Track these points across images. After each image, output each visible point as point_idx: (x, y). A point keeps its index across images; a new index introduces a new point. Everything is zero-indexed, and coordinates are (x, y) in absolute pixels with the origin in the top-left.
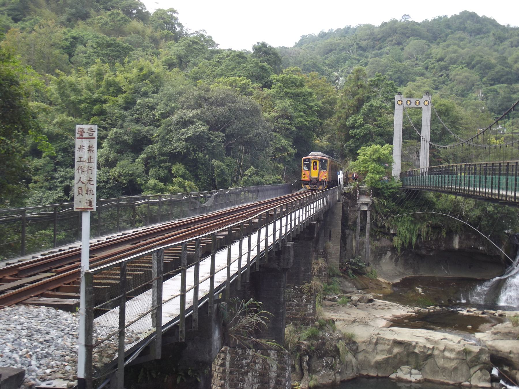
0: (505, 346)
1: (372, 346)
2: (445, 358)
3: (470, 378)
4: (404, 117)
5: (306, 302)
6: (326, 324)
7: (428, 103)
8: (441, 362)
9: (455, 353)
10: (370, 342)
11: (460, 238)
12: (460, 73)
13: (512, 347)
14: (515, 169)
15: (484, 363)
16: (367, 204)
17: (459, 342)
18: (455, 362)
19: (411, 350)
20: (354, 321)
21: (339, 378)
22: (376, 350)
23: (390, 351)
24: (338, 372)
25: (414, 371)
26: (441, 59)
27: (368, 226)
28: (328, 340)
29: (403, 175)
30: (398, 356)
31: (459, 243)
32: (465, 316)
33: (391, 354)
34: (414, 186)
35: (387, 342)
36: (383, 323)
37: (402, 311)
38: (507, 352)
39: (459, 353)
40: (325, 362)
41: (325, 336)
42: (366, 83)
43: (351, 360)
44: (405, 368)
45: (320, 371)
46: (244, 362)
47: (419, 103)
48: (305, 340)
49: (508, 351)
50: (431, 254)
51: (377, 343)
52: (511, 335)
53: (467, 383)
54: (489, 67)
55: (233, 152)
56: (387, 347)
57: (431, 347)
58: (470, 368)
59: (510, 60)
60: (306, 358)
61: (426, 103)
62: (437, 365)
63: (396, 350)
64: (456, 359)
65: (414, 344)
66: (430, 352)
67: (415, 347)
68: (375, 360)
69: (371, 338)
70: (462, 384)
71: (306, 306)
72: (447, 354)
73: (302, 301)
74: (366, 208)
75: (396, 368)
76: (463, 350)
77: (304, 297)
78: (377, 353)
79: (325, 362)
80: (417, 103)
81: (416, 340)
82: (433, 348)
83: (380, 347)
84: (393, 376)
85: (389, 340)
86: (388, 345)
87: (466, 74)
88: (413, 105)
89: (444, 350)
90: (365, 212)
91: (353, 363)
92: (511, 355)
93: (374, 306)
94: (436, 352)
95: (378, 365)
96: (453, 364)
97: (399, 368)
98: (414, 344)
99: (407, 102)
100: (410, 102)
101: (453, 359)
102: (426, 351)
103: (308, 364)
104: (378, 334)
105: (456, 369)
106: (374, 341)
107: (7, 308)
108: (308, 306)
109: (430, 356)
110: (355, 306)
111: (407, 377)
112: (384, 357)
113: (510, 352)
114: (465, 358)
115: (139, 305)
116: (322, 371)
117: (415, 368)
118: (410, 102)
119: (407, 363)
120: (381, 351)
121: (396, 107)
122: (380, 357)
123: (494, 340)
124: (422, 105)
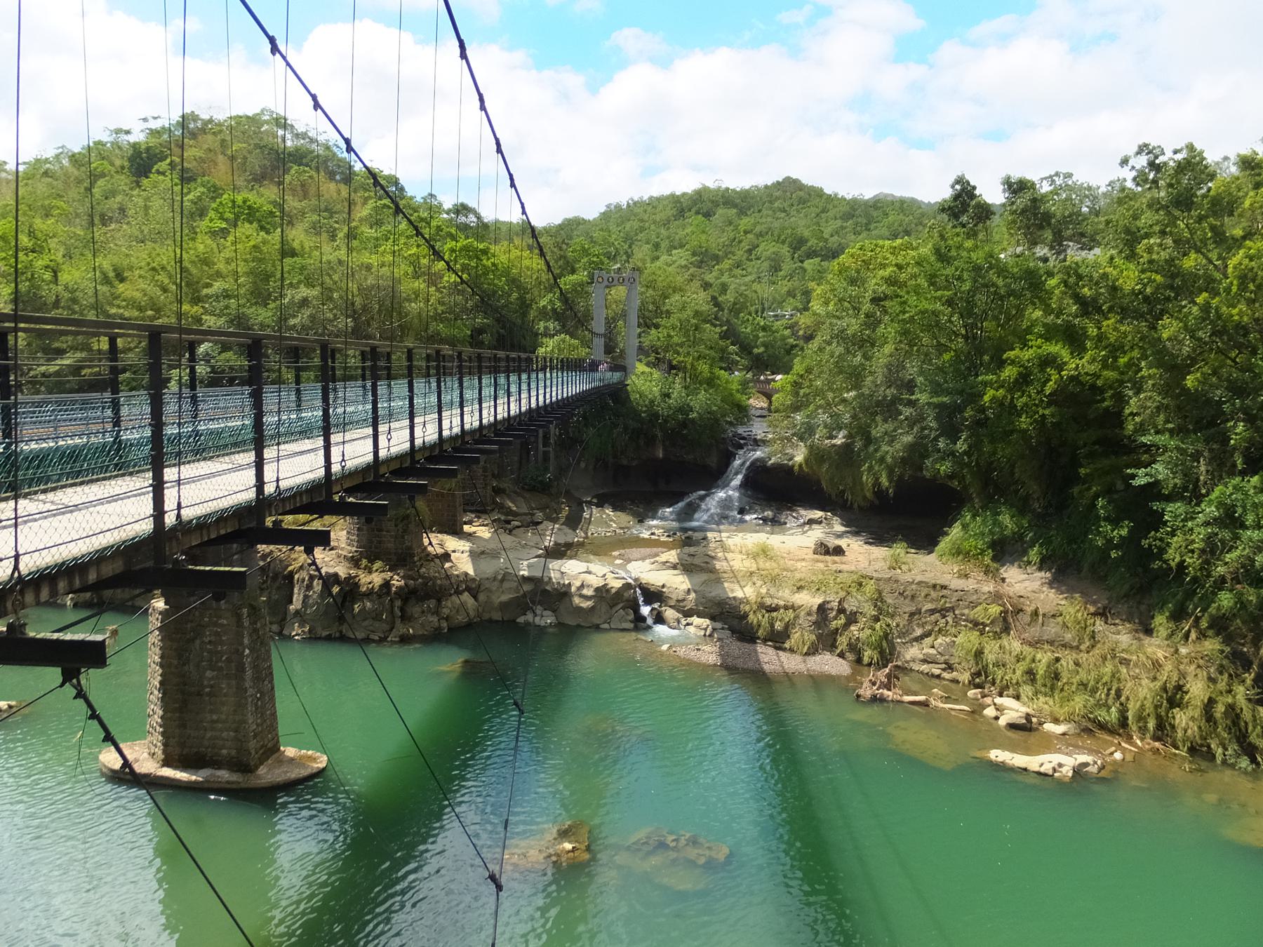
2: (582, 596)
10: (495, 579)
12: (767, 248)
20: (483, 553)
23: (517, 590)
34: (129, 336)
46: (189, 626)
51: (502, 580)
54: (801, 241)
55: (855, 377)
58: (611, 607)
59: (827, 233)
60: (398, 603)
67: (547, 583)
69: (497, 573)
72: (585, 592)
83: (506, 585)
84: (521, 620)
87: (775, 249)
95: (504, 606)
96: (589, 604)
103: (402, 609)
107: (609, 511)
113: (663, 586)
122: (505, 598)
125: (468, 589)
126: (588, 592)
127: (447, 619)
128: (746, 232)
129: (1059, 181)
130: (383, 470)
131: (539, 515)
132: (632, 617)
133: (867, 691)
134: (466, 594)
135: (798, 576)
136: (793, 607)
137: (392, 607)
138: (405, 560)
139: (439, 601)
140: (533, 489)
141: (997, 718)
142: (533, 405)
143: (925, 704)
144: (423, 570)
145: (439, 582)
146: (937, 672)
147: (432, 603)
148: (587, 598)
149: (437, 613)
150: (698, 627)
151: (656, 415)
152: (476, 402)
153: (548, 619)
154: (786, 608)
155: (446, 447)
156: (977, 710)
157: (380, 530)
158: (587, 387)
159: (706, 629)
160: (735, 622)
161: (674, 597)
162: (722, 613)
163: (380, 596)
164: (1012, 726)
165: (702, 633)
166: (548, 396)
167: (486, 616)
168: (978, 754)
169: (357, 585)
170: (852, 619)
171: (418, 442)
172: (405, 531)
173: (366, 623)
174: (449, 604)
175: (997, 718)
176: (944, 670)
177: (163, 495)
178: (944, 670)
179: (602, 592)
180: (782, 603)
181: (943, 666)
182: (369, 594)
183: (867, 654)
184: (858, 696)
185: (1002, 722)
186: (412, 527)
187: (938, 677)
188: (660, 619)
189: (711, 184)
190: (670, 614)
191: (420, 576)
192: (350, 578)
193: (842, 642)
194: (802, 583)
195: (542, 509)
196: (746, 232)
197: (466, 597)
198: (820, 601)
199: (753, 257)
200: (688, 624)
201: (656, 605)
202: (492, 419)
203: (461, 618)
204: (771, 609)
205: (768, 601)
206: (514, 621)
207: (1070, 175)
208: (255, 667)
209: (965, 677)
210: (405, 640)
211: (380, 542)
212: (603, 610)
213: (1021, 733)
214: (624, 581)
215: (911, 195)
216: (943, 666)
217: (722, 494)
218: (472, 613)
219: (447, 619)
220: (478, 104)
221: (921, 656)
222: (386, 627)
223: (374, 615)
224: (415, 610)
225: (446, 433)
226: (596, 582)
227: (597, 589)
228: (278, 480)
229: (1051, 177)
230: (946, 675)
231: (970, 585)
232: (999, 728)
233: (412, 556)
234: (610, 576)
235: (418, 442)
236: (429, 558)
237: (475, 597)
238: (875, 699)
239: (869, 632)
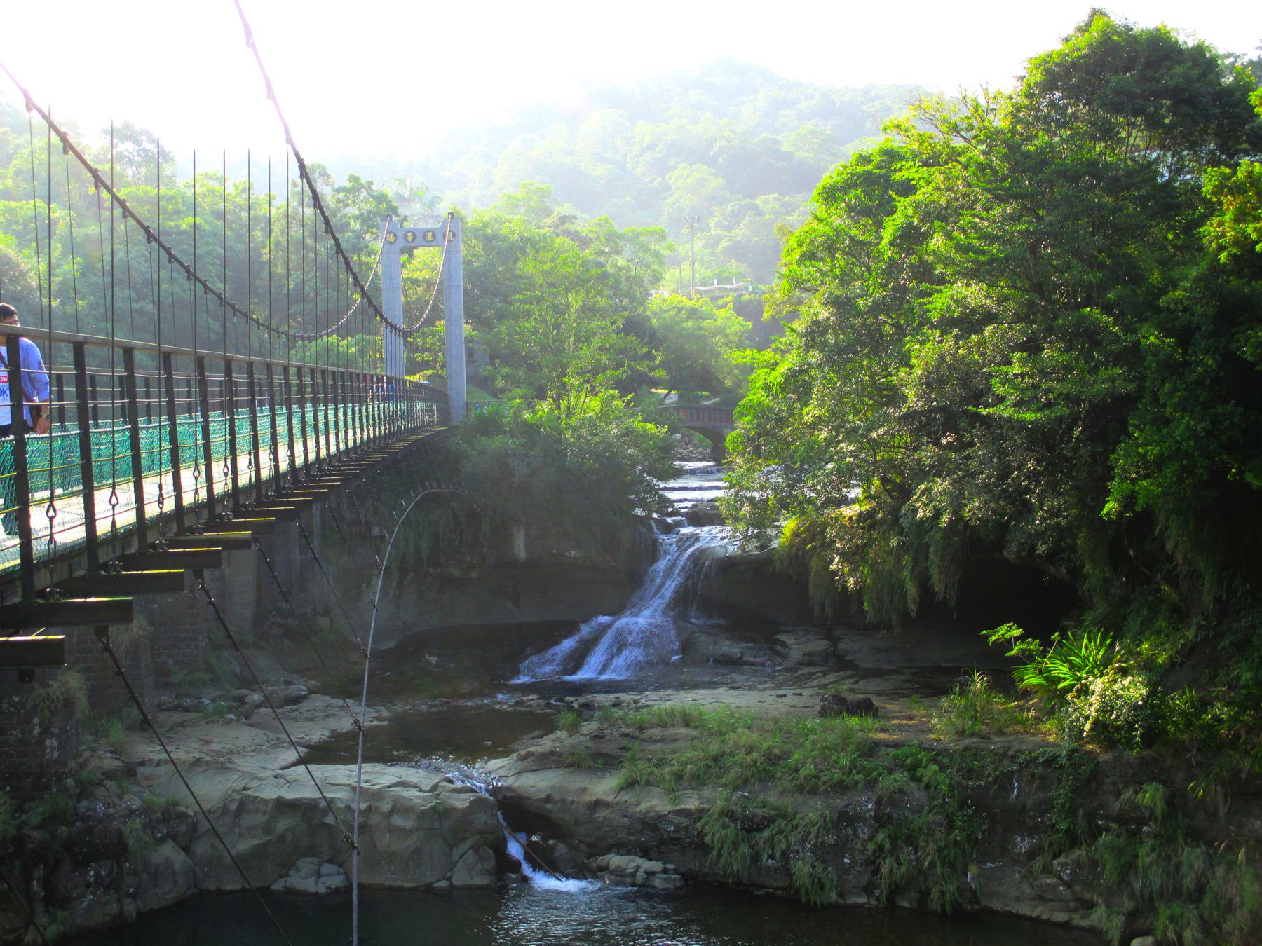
1: (228, 819)
2: (393, 830)
3: (451, 870)
5: (41, 733)
6: (102, 780)
9: (414, 817)
10: (224, 811)
11: (527, 535)
13: (553, 788)
14: (70, 389)
15: (480, 832)
21: (130, 908)
22: (239, 826)
23: (267, 829)
24: (128, 895)
25: (327, 868)
26: (652, 147)
28: (100, 821)
30: (289, 837)
31: (526, 546)
33: (269, 834)
35: (261, 807)
38: (541, 800)
39: (423, 815)
40: (92, 873)
41: (95, 810)
44: (306, 864)
45: (83, 895)
48: (36, 828)
49: (543, 796)
50: (474, 575)
52: (554, 758)
53: (444, 884)
56: (260, 819)
57: (363, 806)
58: (451, 847)
60: (39, 872)
62: (376, 848)
63: (283, 825)
64: (418, 830)
67: (325, 812)
69: (227, 800)
71: (41, 742)
72: (398, 821)
73: (31, 731)
75: (287, 865)
76: (433, 808)
77: (36, 720)
78: (241, 835)
79: (92, 873)
82: (369, 809)
84: (278, 886)
85: (266, 802)
86: (264, 813)
89: (392, 812)
91: (177, 866)
92: (549, 806)
94: (375, 819)
96: (411, 843)
97: (294, 864)
99: (406, 236)
101: (411, 831)
104: (245, 789)
105: (417, 851)
106: (233, 807)
108: (48, 743)
110: (246, 718)
111: (309, 885)
112: (256, 842)
113: (548, 799)
114: (437, 825)
116: (85, 896)
117: (330, 861)
119: (310, 852)
120: (249, 829)
123: (519, 772)
130: (103, 556)
132: (490, 864)
142: (299, 461)
148: (406, 833)
151: (251, 265)
152: (167, 467)
155: (43, 580)
158: (353, 438)
166: (358, 435)
171: (103, 528)
177: (85, 508)
202: (203, 495)
206: (268, 888)
214: (471, 796)
220: (265, 91)
225: (151, 511)
228: (51, 535)
231: (313, 347)
235: (103, 528)
237: (186, 850)
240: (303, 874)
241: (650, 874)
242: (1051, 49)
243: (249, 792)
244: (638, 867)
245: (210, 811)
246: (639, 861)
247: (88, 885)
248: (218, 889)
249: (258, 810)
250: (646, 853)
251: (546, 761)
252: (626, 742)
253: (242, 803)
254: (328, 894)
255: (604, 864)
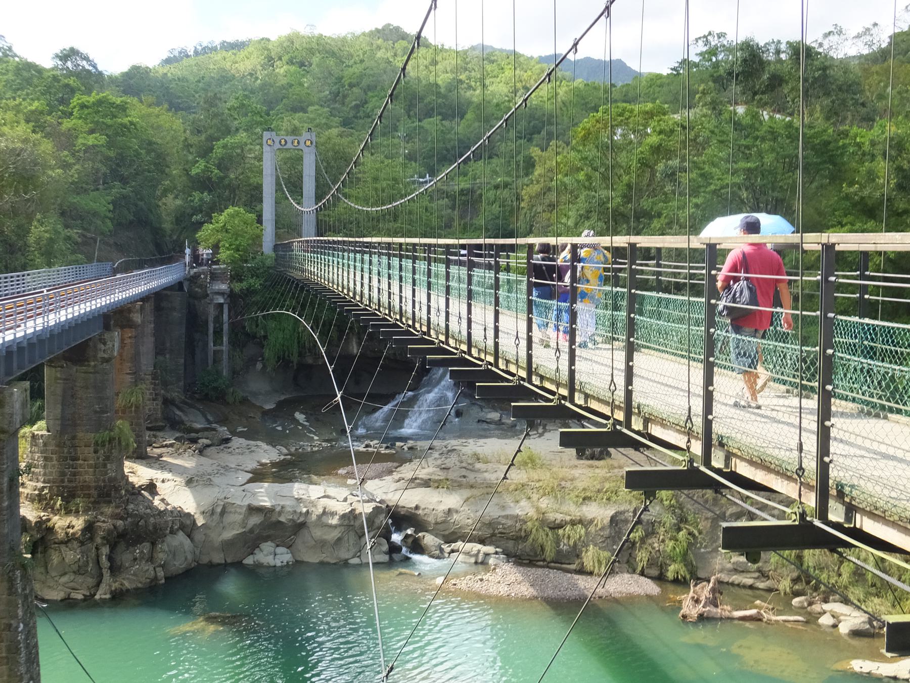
0: (410, 499)
4: (126, 268)
7: (311, 143)
8: (318, 533)
9: (338, 517)
16: (221, 293)
17: (345, 500)
18: (339, 529)
19: (273, 519)
23: (244, 523)
25: (281, 550)
27: (226, 327)
29: (276, 248)
32: (362, 452)
36: (245, 477)
37: (268, 454)
42: (224, 107)
43: (181, 544)
44: (268, 546)
47: (298, 143)
51: (223, 512)
60: (105, 550)
61: (308, 143)
64: (340, 525)
65: (278, 509)
66: (302, 519)
67: (280, 513)
68: (220, 539)
70: (837, 248)
74: (221, 301)
80: (296, 144)
81: (282, 503)
84: (249, 561)
88: (289, 145)
90: (221, 305)
91: (186, 547)
93: (230, 450)
95: (228, 545)
98: (278, 509)
99: (280, 142)
100: (286, 142)
102: (296, 518)
103: (110, 558)
105: (339, 539)
106: (219, 510)
109: (302, 526)
113: (417, 507)
114: (352, 523)
115: (63, 312)
118: (286, 142)
121: (266, 148)
122: (228, 535)
124: (302, 146)
125: (182, 527)
126: (334, 521)
127: (163, 566)
128: (351, 86)
129: (714, 42)
131: (223, 431)
133: (690, 609)
134: (181, 533)
135: (580, 485)
136: (581, 522)
137: (98, 556)
138: (109, 495)
139: (153, 544)
140: (206, 398)
141: (835, 626)
143: (757, 619)
144: (131, 506)
145: (152, 520)
146: (749, 581)
147: (146, 547)
149: (151, 559)
150: (468, 554)
153: (283, 557)
154: (573, 523)
156: (812, 619)
157: (75, 459)
159: (477, 555)
160: (511, 544)
161: (431, 519)
162: (493, 535)
163: (82, 543)
164: (856, 633)
165: (473, 560)
167: (205, 560)
168: (839, 666)
169: (51, 530)
170: (651, 532)
172: (107, 458)
173: (64, 579)
174: (165, 547)
175: (835, 626)
176: (757, 578)
178: (757, 578)
179: (351, 517)
180: (568, 518)
181: (757, 575)
182: (68, 540)
183: (672, 570)
184: (684, 617)
185: (844, 629)
186: (115, 452)
187: (751, 587)
188: (417, 547)
189: (305, 31)
190: (429, 539)
191: (129, 515)
192: (40, 523)
193: (642, 557)
194: (588, 494)
195: (223, 421)
196: (351, 86)
197: (181, 536)
198: (611, 512)
199: (361, 114)
200: (453, 551)
201: (409, 532)
203: (179, 565)
204: (556, 526)
205: (551, 516)
207: (721, 35)
208: (27, 646)
209: (785, 585)
210: (118, 599)
211: (74, 474)
212: (351, 542)
213: (866, 640)
214: (373, 505)
215: (275, 27)
216: (757, 575)
217: (431, 396)
218: (190, 557)
219: (163, 566)
221: (729, 566)
222: (91, 581)
223: (75, 567)
224: (125, 557)
226: (342, 508)
227: (343, 516)
229: (705, 37)
230: (761, 585)
232: (840, 636)
233: (117, 490)
234: (351, 499)
236: (134, 492)
238: (701, 618)
239: (671, 544)
240: (265, 553)
241: (487, 555)
242: (499, 40)
243: (229, 500)
244: (479, 551)
245: (806, 251)
246: (479, 546)
247: (135, 559)
248: (210, 562)
249: (235, 512)
250: (482, 541)
251: (414, 483)
252: (464, 472)
253: (224, 507)
254: (282, 567)
255: (456, 548)
